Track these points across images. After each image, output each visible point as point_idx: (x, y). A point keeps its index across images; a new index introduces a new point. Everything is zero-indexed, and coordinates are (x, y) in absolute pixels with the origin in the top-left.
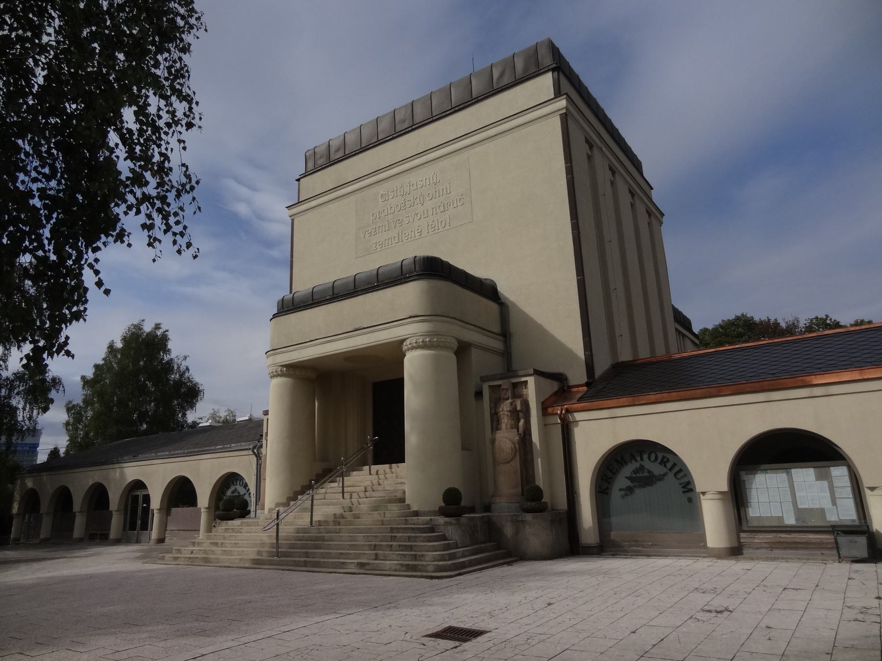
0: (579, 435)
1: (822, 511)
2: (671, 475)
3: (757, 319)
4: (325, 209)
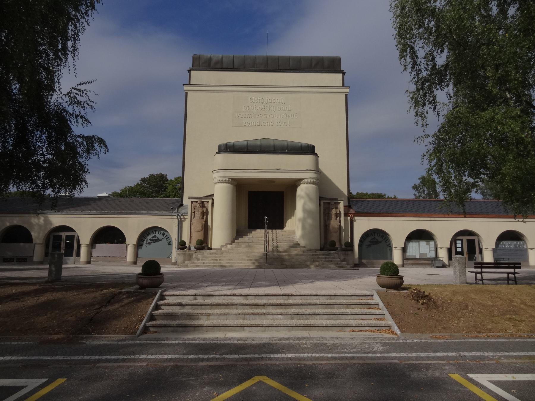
0: (355, 224)
1: (426, 254)
2: (165, 239)
3: (133, 185)
4: (240, 94)
